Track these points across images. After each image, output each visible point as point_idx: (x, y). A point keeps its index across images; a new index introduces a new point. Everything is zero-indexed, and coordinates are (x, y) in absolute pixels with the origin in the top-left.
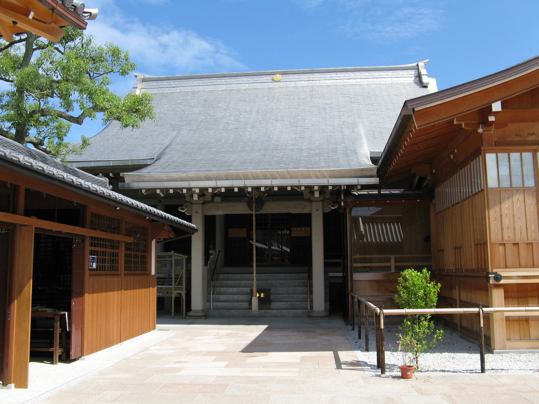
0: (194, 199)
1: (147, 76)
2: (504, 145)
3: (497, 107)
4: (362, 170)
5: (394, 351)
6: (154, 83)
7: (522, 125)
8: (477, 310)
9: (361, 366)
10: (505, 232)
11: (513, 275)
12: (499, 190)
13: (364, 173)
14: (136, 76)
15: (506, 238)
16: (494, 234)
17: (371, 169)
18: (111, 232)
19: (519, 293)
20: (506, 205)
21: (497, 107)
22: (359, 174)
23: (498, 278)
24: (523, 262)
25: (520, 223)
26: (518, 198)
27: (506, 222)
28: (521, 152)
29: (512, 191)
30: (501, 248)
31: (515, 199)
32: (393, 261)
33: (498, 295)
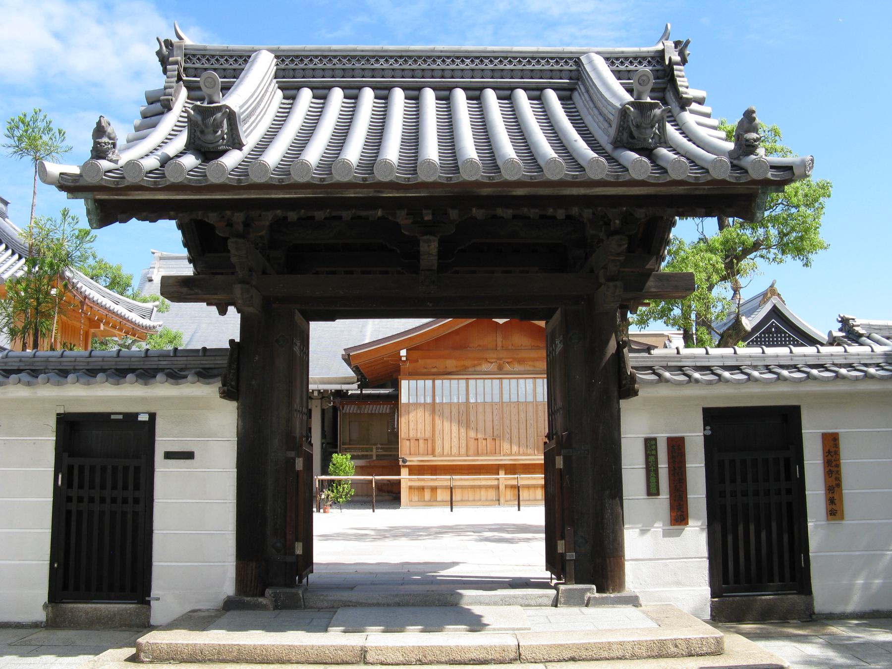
0: (426, 218)
1: (165, 254)
2: (415, 374)
3: (403, 353)
4: (346, 378)
5: (65, 414)
6: (173, 262)
7: (428, 361)
8: (370, 477)
9: (355, 535)
10: (419, 432)
11: (414, 460)
12: (408, 405)
13: (347, 380)
14: (153, 253)
15: (411, 436)
16: (403, 433)
17: (353, 378)
18: (293, 646)
19: (416, 470)
20: (412, 415)
21: (403, 353)
22: (343, 381)
23: (404, 461)
24: (421, 452)
25: (420, 426)
26: (420, 412)
27: (412, 426)
28: (425, 379)
29: (417, 405)
30: (484, 442)
31: (418, 411)
32: (374, 450)
33: (404, 472)
